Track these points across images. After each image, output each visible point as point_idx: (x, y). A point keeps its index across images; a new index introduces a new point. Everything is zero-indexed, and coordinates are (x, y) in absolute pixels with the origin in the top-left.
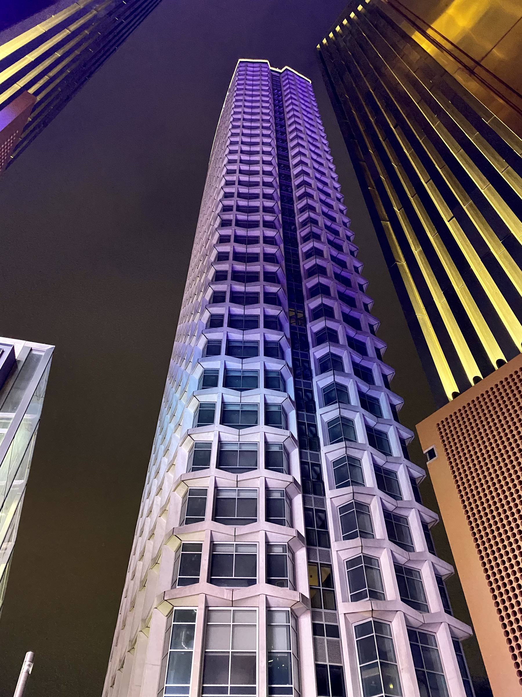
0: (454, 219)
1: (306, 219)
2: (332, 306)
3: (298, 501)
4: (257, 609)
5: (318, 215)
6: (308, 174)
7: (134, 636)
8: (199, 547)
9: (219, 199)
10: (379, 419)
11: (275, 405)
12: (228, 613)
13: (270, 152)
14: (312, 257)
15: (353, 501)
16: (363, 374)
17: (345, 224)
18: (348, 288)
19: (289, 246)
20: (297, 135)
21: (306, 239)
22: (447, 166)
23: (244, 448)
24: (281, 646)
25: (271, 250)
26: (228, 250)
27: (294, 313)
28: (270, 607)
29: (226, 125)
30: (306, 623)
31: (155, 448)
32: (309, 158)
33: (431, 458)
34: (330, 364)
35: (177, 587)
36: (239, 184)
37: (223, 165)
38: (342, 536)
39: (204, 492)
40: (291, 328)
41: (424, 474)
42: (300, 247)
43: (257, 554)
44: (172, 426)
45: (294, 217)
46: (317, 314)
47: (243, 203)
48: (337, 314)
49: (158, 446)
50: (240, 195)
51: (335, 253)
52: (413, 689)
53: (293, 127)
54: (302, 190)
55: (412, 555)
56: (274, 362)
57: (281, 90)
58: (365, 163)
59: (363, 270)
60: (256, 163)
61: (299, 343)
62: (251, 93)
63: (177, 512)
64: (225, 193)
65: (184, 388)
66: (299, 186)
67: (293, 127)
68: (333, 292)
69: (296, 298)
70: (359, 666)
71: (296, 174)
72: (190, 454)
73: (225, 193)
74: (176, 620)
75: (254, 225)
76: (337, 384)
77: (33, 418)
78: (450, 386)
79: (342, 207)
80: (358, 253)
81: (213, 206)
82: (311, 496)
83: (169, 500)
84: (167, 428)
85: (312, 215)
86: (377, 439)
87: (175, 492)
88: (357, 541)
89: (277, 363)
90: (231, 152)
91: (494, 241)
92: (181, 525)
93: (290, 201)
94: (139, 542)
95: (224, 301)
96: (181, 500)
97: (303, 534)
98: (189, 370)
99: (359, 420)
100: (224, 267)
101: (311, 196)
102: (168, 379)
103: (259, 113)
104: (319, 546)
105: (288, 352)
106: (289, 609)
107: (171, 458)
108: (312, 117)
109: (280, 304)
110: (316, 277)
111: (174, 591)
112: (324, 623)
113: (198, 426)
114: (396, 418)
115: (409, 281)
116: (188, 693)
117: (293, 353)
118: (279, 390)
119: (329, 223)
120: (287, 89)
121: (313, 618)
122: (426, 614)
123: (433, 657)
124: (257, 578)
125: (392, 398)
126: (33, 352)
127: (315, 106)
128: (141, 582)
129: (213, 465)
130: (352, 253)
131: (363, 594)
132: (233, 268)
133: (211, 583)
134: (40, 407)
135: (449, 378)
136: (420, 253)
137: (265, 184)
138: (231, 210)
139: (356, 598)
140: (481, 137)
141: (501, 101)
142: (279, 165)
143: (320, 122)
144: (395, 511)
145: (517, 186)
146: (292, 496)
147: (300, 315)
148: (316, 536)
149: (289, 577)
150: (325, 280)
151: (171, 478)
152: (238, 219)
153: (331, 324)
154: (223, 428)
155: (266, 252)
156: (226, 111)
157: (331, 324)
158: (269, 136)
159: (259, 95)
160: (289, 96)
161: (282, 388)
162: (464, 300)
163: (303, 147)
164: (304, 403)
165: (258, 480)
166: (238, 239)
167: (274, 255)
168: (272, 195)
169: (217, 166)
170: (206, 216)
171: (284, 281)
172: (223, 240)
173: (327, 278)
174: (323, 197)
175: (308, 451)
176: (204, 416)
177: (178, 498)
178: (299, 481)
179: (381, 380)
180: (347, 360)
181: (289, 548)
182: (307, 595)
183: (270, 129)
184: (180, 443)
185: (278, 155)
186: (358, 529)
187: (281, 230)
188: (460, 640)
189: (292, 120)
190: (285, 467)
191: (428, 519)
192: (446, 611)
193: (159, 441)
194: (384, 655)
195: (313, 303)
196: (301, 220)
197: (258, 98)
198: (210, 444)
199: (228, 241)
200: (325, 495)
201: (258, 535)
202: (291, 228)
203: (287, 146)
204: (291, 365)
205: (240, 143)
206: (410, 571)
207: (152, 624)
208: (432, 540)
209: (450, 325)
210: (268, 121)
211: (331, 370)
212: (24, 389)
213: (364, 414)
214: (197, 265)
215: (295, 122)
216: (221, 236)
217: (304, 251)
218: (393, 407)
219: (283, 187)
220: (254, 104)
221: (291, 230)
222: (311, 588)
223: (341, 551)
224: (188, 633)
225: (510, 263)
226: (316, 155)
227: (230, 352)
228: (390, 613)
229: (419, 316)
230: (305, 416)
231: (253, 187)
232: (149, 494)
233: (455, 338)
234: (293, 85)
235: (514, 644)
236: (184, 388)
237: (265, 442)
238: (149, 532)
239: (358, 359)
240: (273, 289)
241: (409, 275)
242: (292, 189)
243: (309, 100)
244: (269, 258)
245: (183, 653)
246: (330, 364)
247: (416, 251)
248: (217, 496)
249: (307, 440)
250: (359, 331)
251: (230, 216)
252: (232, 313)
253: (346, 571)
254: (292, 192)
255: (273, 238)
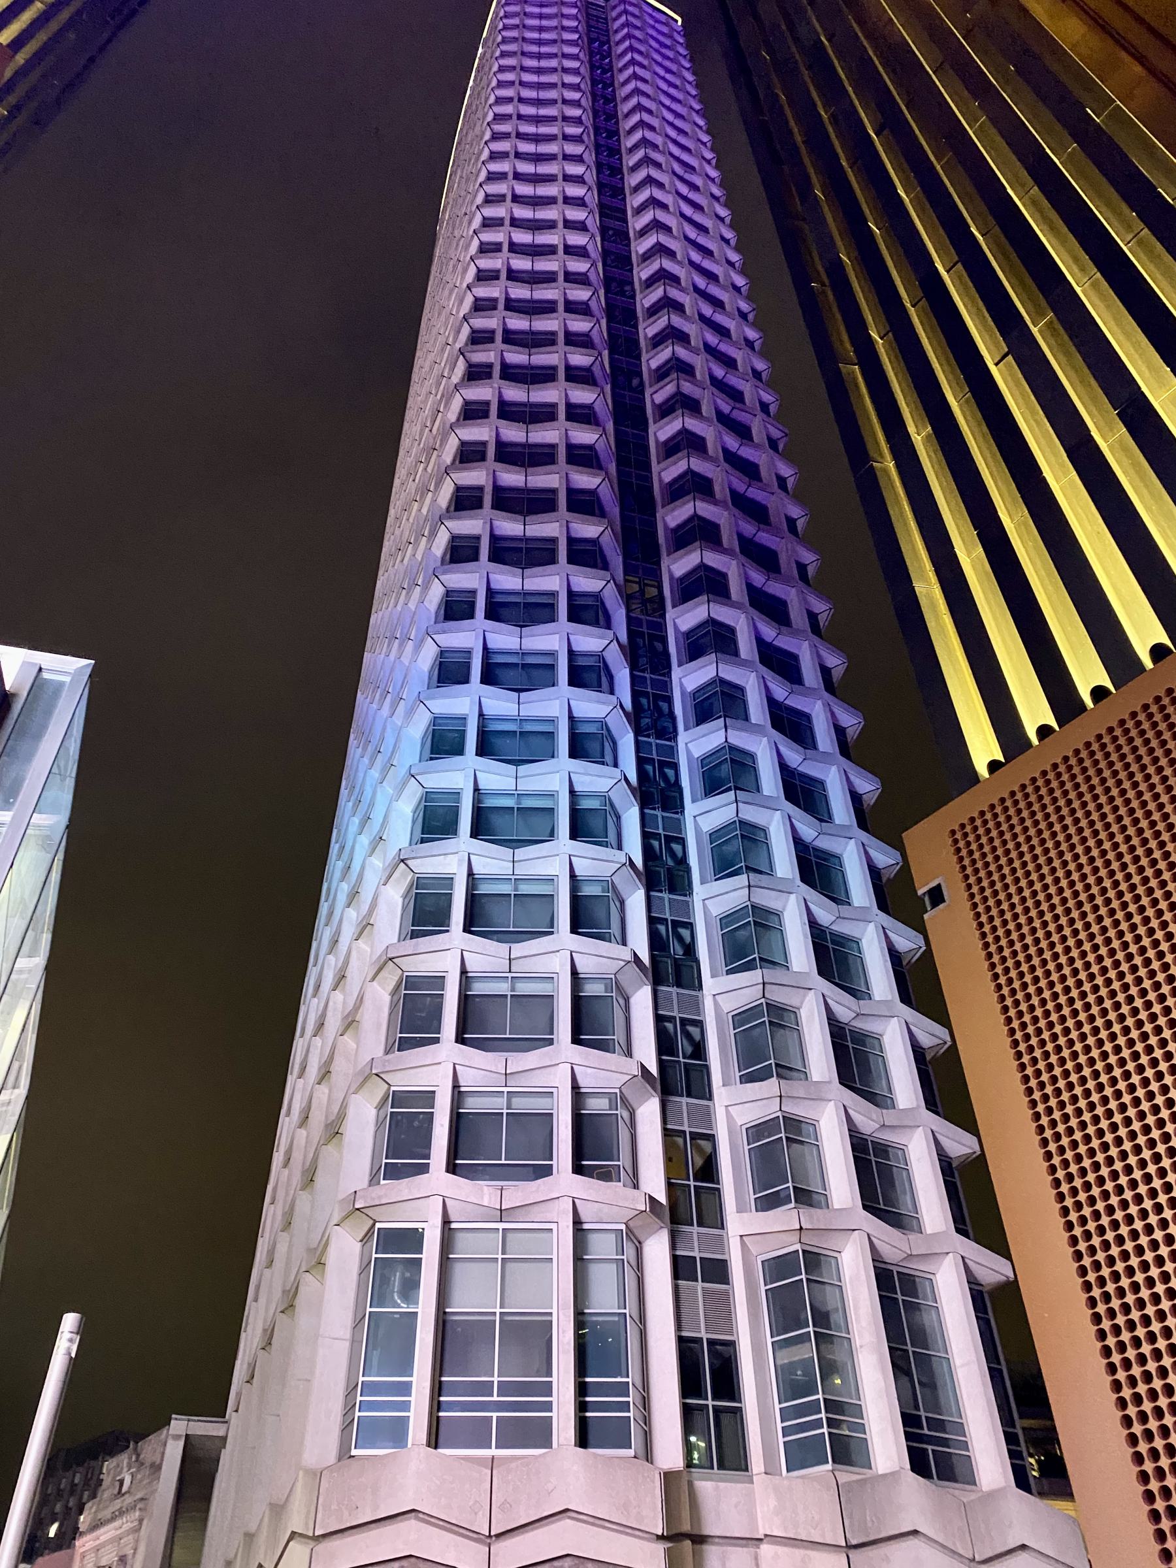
0: (1010, 357)
1: (667, 362)
2: (724, 570)
3: (642, 1000)
4: (553, 1226)
5: (696, 351)
6: (671, 254)
7: (292, 1278)
8: (428, 1097)
9: (461, 315)
10: (824, 824)
11: (591, 881)
12: (492, 1235)
13: (582, 199)
14: (680, 454)
15: (763, 1000)
16: (790, 724)
17: (757, 374)
18: (762, 526)
19: (627, 426)
20: (639, 104)
21: (665, 410)
22: (997, 228)
23: (525, 889)
24: (604, 1300)
25: (585, 436)
26: (485, 438)
27: (636, 587)
28: (582, 1223)
29: (478, 129)
30: (657, 1251)
31: (329, 889)
32: (673, 214)
33: (935, 904)
34: (719, 702)
35: (382, 1182)
36: (509, 278)
37: (471, 232)
38: (738, 1074)
39: (439, 981)
40: (630, 620)
41: (922, 943)
42: (652, 428)
43: (554, 1112)
44: (364, 840)
45: (639, 357)
46: (689, 589)
47: (518, 323)
48: (736, 589)
49: (336, 887)
50: (512, 305)
51: (732, 443)
52: (883, 1384)
53: (638, 135)
54: (657, 293)
55: (889, 1117)
56: (589, 701)
57: (608, 42)
58: (806, 227)
59: (819, 571)
60: (550, 201)
61: (648, 654)
62: (536, 35)
63: (379, 1025)
64: (477, 299)
65: (390, 758)
66: (650, 283)
67: (638, 135)
68: (727, 537)
69: (641, 549)
70: (769, 1340)
71: (647, 280)
72: (407, 901)
73: (477, 299)
74: (380, 1248)
75: (545, 340)
76: (733, 749)
77: (53, 821)
78: (983, 746)
79: (752, 334)
80: (756, 316)
81: (449, 333)
82: (651, 740)
83: (360, 1000)
84: (353, 847)
85: (682, 353)
86: (817, 870)
87: (375, 983)
88: (771, 1086)
89: (599, 702)
90: (489, 200)
91: (1099, 411)
92: (387, 1052)
93: (629, 316)
94: (297, 1090)
95: (475, 558)
96: (387, 999)
97: (653, 1069)
98: (398, 720)
99: (793, 911)
100: (475, 476)
101: (679, 307)
102: (352, 736)
103: (554, 102)
104: (689, 1095)
105: (623, 676)
106: (623, 1227)
107: (365, 908)
108: (680, 96)
109: (602, 514)
110: (689, 501)
111: (376, 1191)
112: (696, 1254)
113: (423, 841)
114: (862, 824)
115: (906, 524)
116: (411, 1376)
117: (634, 680)
118: (603, 763)
119: (719, 372)
120: (619, 15)
121: (673, 1246)
122: (912, 1237)
123: (927, 1323)
124: (554, 1163)
125: (823, 653)
126: (45, 675)
127: (690, 83)
128: (304, 1172)
129: (457, 924)
130: (773, 444)
131: (782, 1195)
132: (498, 435)
133: (454, 1173)
134: (67, 797)
135: (984, 734)
136: (927, 439)
137: (569, 250)
138: (491, 340)
139: (768, 1203)
140: (1081, 155)
141: (1138, 69)
142: (603, 230)
143: (701, 122)
144: (853, 1023)
145: (1159, 276)
146: (629, 991)
147: (652, 592)
148: (680, 1072)
149: (624, 1160)
150: (712, 508)
151: (364, 954)
152: (507, 361)
153: (713, 559)
154: (477, 845)
155: (574, 441)
156: (476, 95)
157: (713, 559)
158: (578, 159)
159: (555, 55)
160: (628, 57)
161: (609, 758)
162: (1023, 550)
163: (661, 186)
164: (657, 791)
165: (553, 958)
166: (508, 411)
167: (591, 447)
168: (586, 303)
169: (456, 233)
170: (431, 357)
171: (614, 511)
172: (473, 412)
173: (716, 503)
174: (707, 310)
175: (659, 813)
176: (436, 822)
177: (380, 999)
178: (645, 957)
179: (832, 741)
180: (746, 634)
181: (622, 1100)
182: (662, 1198)
183: (582, 141)
184: (384, 878)
185: (601, 206)
186: (772, 1061)
187: (608, 388)
188: (985, 1290)
189: (635, 118)
190: (615, 929)
191: (926, 1041)
192: (958, 1231)
193: (337, 874)
194: (822, 1318)
195: (680, 565)
196: (654, 364)
197: (553, 63)
198: (449, 881)
199: (485, 414)
200: (700, 987)
201: (555, 1071)
202: (631, 382)
203: (620, 145)
204: (628, 705)
205: (511, 176)
206: (861, 1038)
207: (332, 1257)
208: (936, 1092)
209: (990, 608)
210: (578, 121)
211: (720, 717)
212: (29, 757)
213: (791, 814)
214: (411, 473)
215: (642, 124)
216: (467, 403)
217: (672, 524)
218: (856, 798)
219: (614, 285)
220: (544, 79)
221: (631, 389)
222: (670, 1186)
223: (735, 1107)
224: (408, 1275)
225: (1135, 465)
226: (691, 212)
227: (495, 611)
228: (837, 1234)
229: (919, 587)
230: (660, 819)
231: (541, 286)
232: (318, 987)
233: (999, 639)
234: (637, 28)
235: (1154, 1486)
236: (390, 758)
237: (573, 1088)
238: (320, 1069)
239: (780, 692)
240: (588, 529)
241: (913, 524)
242: (633, 290)
243: (674, 67)
244: (581, 457)
245: (397, 1316)
246: (718, 704)
247: (919, 435)
248: (466, 990)
249: (664, 872)
250: (783, 628)
251: (486, 355)
252: (497, 532)
253: (747, 1148)
254: (633, 297)
255: (590, 407)
